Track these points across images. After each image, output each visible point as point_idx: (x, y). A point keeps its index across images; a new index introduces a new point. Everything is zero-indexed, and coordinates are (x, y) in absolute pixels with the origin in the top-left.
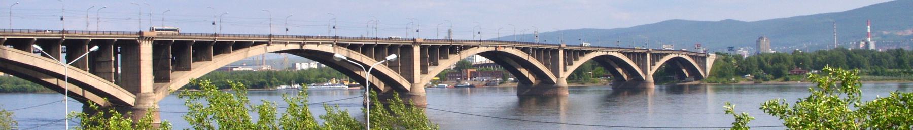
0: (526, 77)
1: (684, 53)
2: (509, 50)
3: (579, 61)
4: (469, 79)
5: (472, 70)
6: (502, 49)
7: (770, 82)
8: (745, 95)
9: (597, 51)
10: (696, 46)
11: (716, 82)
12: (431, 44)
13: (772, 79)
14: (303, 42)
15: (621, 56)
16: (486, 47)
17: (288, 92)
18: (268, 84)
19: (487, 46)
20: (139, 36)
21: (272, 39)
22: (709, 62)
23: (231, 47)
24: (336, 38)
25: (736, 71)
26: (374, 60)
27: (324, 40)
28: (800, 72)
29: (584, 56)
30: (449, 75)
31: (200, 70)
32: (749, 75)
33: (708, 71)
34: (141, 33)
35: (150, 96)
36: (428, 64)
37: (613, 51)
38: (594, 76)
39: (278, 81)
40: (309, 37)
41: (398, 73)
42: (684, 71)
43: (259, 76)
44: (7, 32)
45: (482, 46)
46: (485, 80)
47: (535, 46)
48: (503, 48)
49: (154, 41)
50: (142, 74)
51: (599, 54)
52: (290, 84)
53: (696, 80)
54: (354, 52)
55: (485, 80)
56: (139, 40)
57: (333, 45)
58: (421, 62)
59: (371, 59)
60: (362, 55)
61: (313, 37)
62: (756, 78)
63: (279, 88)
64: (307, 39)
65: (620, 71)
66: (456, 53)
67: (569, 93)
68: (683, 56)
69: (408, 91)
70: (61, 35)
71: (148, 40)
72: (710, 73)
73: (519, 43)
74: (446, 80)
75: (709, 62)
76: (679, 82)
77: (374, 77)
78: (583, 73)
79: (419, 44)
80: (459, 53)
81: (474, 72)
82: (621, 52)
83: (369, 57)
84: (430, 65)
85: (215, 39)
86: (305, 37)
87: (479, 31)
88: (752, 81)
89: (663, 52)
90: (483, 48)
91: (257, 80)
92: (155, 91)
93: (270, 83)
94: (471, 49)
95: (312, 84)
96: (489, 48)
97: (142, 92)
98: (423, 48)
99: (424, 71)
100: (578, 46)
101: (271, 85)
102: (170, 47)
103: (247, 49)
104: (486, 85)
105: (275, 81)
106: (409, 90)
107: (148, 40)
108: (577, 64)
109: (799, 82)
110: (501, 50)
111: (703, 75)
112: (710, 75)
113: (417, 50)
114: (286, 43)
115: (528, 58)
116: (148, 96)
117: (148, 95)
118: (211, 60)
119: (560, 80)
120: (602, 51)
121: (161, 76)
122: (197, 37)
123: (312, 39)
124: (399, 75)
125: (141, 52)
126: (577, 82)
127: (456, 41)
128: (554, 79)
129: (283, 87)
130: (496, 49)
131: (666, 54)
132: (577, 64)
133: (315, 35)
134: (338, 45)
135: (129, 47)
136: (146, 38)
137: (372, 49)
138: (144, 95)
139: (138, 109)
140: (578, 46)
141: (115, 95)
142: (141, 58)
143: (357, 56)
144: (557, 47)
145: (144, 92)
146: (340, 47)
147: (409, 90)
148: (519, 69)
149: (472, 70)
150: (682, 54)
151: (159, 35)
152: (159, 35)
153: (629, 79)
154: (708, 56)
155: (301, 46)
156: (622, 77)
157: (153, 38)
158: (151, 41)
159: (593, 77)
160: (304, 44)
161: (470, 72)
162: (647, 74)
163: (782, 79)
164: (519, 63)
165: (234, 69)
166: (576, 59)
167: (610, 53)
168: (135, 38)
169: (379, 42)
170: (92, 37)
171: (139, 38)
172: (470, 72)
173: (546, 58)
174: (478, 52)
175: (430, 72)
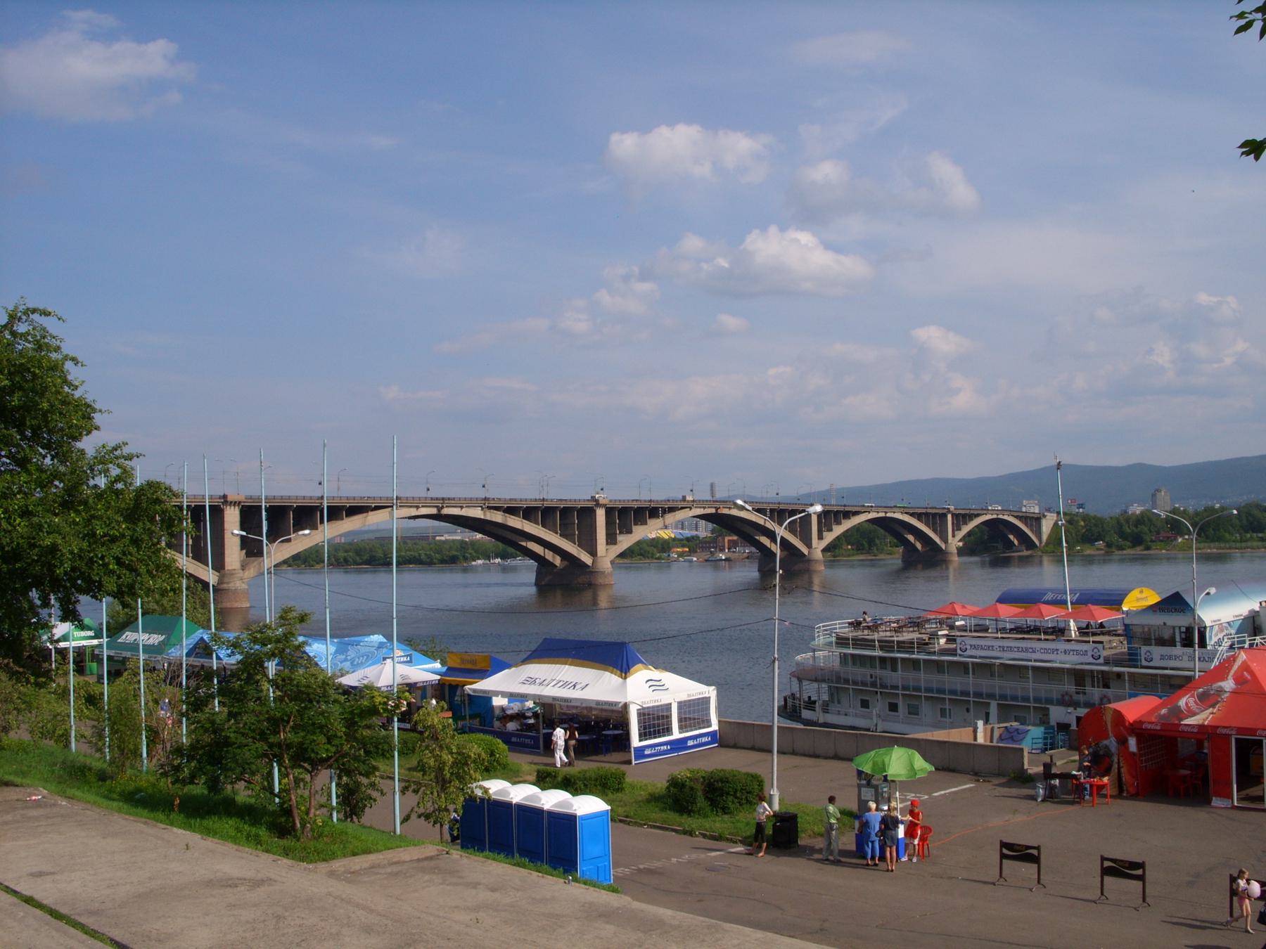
0: (767, 548)
1: (1006, 513)
2: (898, 516)
3: (842, 525)
4: (727, 550)
5: (730, 538)
7: (1125, 552)
8: (1017, 570)
9: (869, 512)
10: (1069, 501)
11: (1053, 552)
12: (620, 506)
13: (1129, 547)
14: (441, 505)
15: (907, 518)
16: (702, 509)
17: (486, 568)
18: (461, 558)
19: (704, 508)
20: (222, 501)
22: (1046, 526)
23: (344, 513)
24: (486, 499)
25: (1083, 536)
26: (540, 527)
27: (471, 503)
28: (1168, 538)
29: (850, 519)
30: (701, 545)
31: (304, 540)
32: (1101, 542)
33: (1045, 537)
34: (225, 497)
35: (236, 574)
36: (618, 532)
37: (894, 512)
38: (892, 544)
39: (474, 554)
40: (449, 499)
41: (575, 544)
42: (1011, 537)
43: (451, 547)
45: (696, 507)
46: (747, 551)
47: (775, 507)
48: (728, 509)
49: (242, 506)
50: (226, 547)
51: (988, 517)
52: (488, 558)
53: (1027, 550)
54: (512, 516)
55: (747, 551)
56: (223, 505)
57: (482, 509)
58: (607, 529)
59: (536, 526)
60: (524, 521)
61: (454, 499)
62: (1109, 545)
63: (474, 563)
64: (446, 502)
65: (911, 538)
66: (658, 517)
67: (826, 568)
68: (1005, 517)
69: (589, 566)
71: (234, 505)
72: (1047, 540)
73: (784, 504)
74: (696, 552)
75: (1046, 526)
76: (1004, 552)
77: (546, 550)
78: (876, 540)
79: (235, 503)
80: (662, 516)
81: (733, 541)
82: (906, 513)
83: (535, 523)
84: (621, 533)
85: (543, 504)
86: (443, 499)
87: (483, 483)
88: (1101, 549)
89: (972, 512)
90: (698, 509)
91: (447, 553)
92: (243, 567)
93: (464, 556)
94: (680, 511)
95: (518, 558)
96: (871, 514)
97: (226, 569)
98: (610, 511)
99: (820, 537)
100: (841, 506)
101: (466, 559)
103: (365, 515)
104: (748, 558)
105: (470, 554)
106: (591, 565)
107: (234, 505)
108: (838, 530)
109: (1164, 551)
110: (724, 512)
111: (1037, 543)
112: (1048, 543)
113: (601, 515)
114: (417, 507)
115: (765, 523)
116: (233, 574)
117: (234, 572)
118: (317, 529)
119: (813, 551)
120: (878, 512)
121: (252, 549)
122: (298, 501)
123: (453, 502)
124: (576, 546)
125: (225, 519)
126: (868, 553)
127: (657, 501)
128: (805, 550)
129: (480, 562)
130: (717, 511)
131: (978, 515)
133: (457, 496)
134: (489, 508)
135: (587, 513)
136: (231, 502)
137: (538, 513)
138: (228, 572)
139: (220, 590)
140: (841, 506)
142: (225, 528)
143: (516, 522)
144: (945, 511)
145: (230, 568)
146: (492, 511)
147: (591, 565)
148: (757, 538)
149: (730, 538)
150: (1003, 515)
151: (249, 499)
152: (249, 499)
153: (924, 549)
154: (1045, 516)
155: (439, 511)
156: (914, 546)
157: (240, 502)
158: (238, 505)
159: (891, 547)
160: (443, 507)
161: (729, 541)
162: (948, 542)
163: (1141, 548)
164: (905, 529)
165: (438, 538)
166: (839, 523)
167: (888, 515)
168: (218, 502)
169: (546, 504)
170: (195, 502)
171: (222, 502)
172: (729, 541)
173: (935, 523)
175: (620, 542)
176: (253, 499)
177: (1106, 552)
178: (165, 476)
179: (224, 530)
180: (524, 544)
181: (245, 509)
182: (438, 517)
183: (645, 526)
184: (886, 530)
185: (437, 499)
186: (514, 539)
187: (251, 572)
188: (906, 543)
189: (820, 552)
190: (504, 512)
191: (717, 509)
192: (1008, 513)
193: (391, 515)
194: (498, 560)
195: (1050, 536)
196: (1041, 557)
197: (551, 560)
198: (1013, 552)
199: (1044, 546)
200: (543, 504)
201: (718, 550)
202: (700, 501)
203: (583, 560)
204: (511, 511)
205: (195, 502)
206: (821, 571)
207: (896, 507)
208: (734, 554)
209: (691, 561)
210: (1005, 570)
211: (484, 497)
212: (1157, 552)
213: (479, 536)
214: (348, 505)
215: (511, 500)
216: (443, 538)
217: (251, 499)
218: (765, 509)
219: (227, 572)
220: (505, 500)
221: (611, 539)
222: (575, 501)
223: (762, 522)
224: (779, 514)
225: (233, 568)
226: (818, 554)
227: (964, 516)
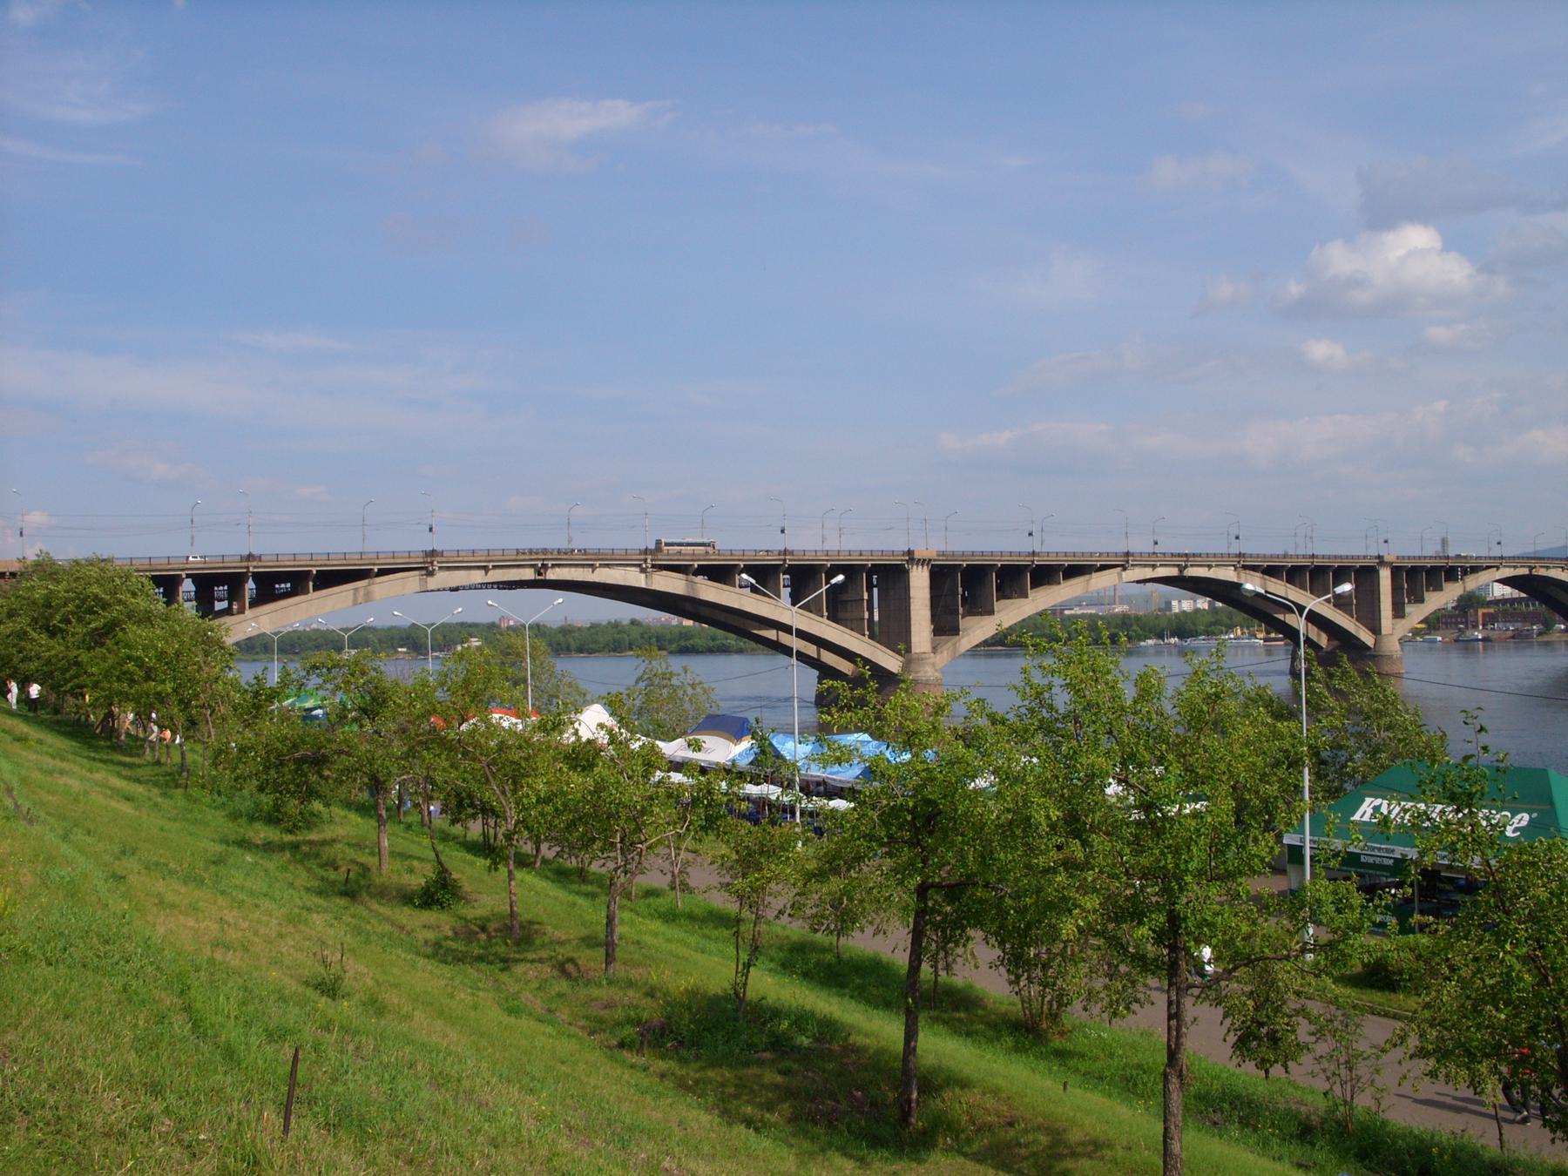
4: (1481, 627)
5: (1486, 611)
17: (1158, 651)
19: (1515, 567)
23: (311, 584)
24: (1240, 555)
26: (1308, 594)
27: (1220, 560)
31: (1010, 613)
34: (910, 553)
36: (1406, 600)
39: (1140, 632)
40: (1194, 555)
50: (913, 622)
52: (1161, 636)
54: (1272, 579)
60: (1288, 585)
61: (1200, 555)
63: (1143, 644)
69: (1369, 648)
70: (783, 557)
79: (923, 562)
84: (1409, 602)
85: (1033, 561)
90: (1508, 569)
92: (935, 649)
98: (1396, 571)
104: (1513, 637)
113: (1385, 575)
114: (1154, 567)
116: (922, 659)
117: (923, 656)
118: (1027, 597)
121: (944, 626)
123: (565, 557)
124: (1354, 620)
125: (911, 584)
128: (1366, 637)
129: (1150, 642)
130: (1530, 571)
133: (1204, 551)
134: (1245, 567)
135: (891, 576)
136: (919, 560)
143: (1279, 588)
145: (918, 651)
149: (1486, 611)
155: (1181, 571)
157: (930, 560)
160: (1186, 566)
161: (1484, 614)
165: (1067, 612)
166: (1439, 588)
169: (1317, 562)
170: (379, 564)
172: (1484, 614)
174: (1497, 578)
176: (602, 554)
178: (1154, 532)
179: (909, 598)
180: (1281, 617)
181: (936, 569)
183: (1441, 593)
184: (724, 630)
186: (1268, 611)
187: (942, 658)
190: (1262, 573)
191: (1531, 568)
194: (1174, 640)
200: (1033, 561)
202: (1509, 558)
203: (1362, 639)
205: (379, 564)
208: (1493, 632)
209: (1434, 641)
211: (1031, 551)
213: (688, 623)
214: (1066, 564)
216: (1072, 612)
217: (943, 555)
219: (914, 656)
221: (1398, 612)
222: (1353, 557)
224: (1316, 575)
225: (922, 651)
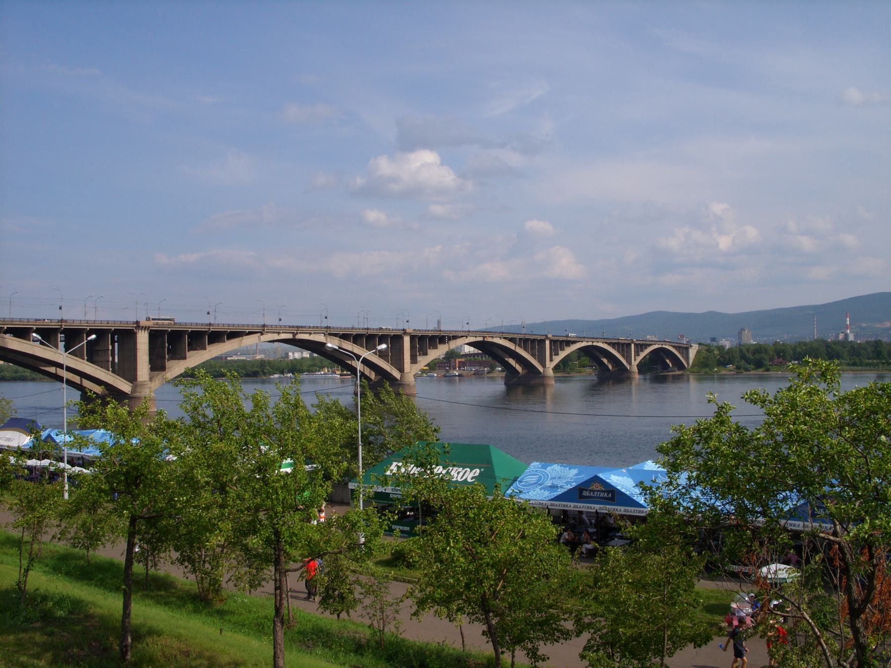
2: (600, 345)
5: (460, 360)
6: (490, 340)
7: (751, 373)
11: (698, 372)
13: (753, 369)
15: (606, 346)
17: (281, 381)
18: (261, 373)
19: (476, 337)
21: (266, 328)
24: (327, 327)
26: (365, 350)
27: (316, 330)
31: (195, 359)
33: (691, 361)
34: (137, 322)
39: (271, 370)
42: (668, 361)
44: (7, 321)
52: (282, 373)
53: (678, 370)
57: (325, 335)
61: (305, 327)
62: (738, 368)
63: (272, 377)
65: (605, 361)
66: (445, 343)
67: (556, 383)
68: (667, 347)
70: (60, 324)
71: (145, 330)
73: (506, 333)
74: (435, 370)
75: (692, 353)
76: (662, 372)
79: (144, 328)
81: (462, 362)
82: (606, 343)
84: (420, 355)
85: (209, 329)
86: (297, 327)
90: (472, 338)
92: (151, 379)
93: (263, 372)
96: (469, 338)
98: (413, 338)
99: (414, 360)
100: (564, 337)
101: (264, 374)
102: (110, 335)
103: (241, 338)
104: (474, 374)
107: (145, 330)
108: (563, 354)
109: (780, 372)
111: (686, 366)
112: (693, 366)
113: (407, 340)
114: (279, 333)
116: (144, 385)
117: (144, 383)
118: (206, 349)
119: (546, 369)
121: (157, 365)
124: (389, 364)
127: (445, 331)
128: (541, 369)
129: (276, 376)
132: (563, 354)
134: (330, 334)
136: (143, 327)
141: (112, 384)
143: (348, 346)
144: (543, 338)
145: (141, 380)
148: (507, 359)
149: (460, 360)
154: (691, 346)
155: (294, 336)
157: (149, 327)
160: (297, 333)
161: (459, 362)
163: (763, 369)
164: (602, 354)
165: (229, 358)
166: (563, 349)
167: (594, 344)
168: (132, 327)
169: (370, 332)
171: (136, 327)
172: (459, 362)
173: (533, 348)
175: (420, 361)
177: (737, 373)
178: (159, 309)
179: (136, 349)
182: (293, 342)
185: (293, 327)
186: (342, 359)
188: (507, 367)
189: (551, 371)
192: (669, 344)
193: (259, 338)
195: (694, 361)
196: (688, 375)
197: (368, 375)
198: (669, 372)
199: (691, 368)
200: (209, 329)
201: (452, 368)
203: (394, 375)
204: (48, 335)
206: (553, 386)
207: (665, 341)
209: (433, 376)
210: (665, 385)
211: (209, 323)
212: (774, 372)
215: (345, 328)
218: (515, 339)
220: (4, 321)
223: (513, 348)
226: (550, 372)
227: (641, 345)
